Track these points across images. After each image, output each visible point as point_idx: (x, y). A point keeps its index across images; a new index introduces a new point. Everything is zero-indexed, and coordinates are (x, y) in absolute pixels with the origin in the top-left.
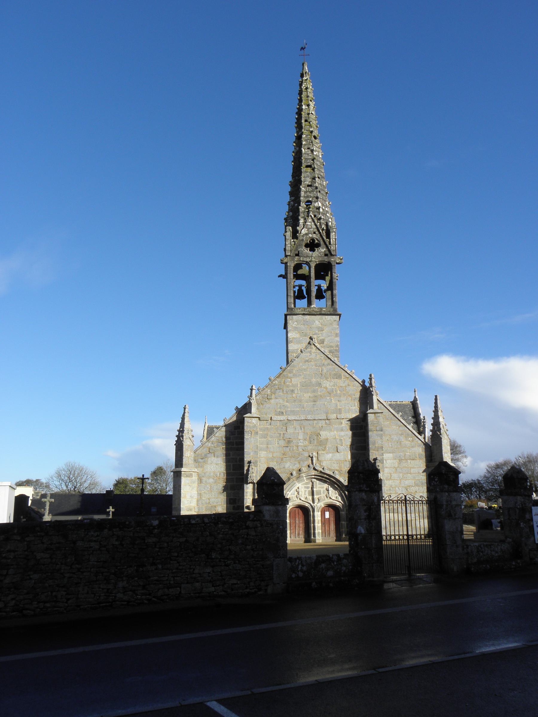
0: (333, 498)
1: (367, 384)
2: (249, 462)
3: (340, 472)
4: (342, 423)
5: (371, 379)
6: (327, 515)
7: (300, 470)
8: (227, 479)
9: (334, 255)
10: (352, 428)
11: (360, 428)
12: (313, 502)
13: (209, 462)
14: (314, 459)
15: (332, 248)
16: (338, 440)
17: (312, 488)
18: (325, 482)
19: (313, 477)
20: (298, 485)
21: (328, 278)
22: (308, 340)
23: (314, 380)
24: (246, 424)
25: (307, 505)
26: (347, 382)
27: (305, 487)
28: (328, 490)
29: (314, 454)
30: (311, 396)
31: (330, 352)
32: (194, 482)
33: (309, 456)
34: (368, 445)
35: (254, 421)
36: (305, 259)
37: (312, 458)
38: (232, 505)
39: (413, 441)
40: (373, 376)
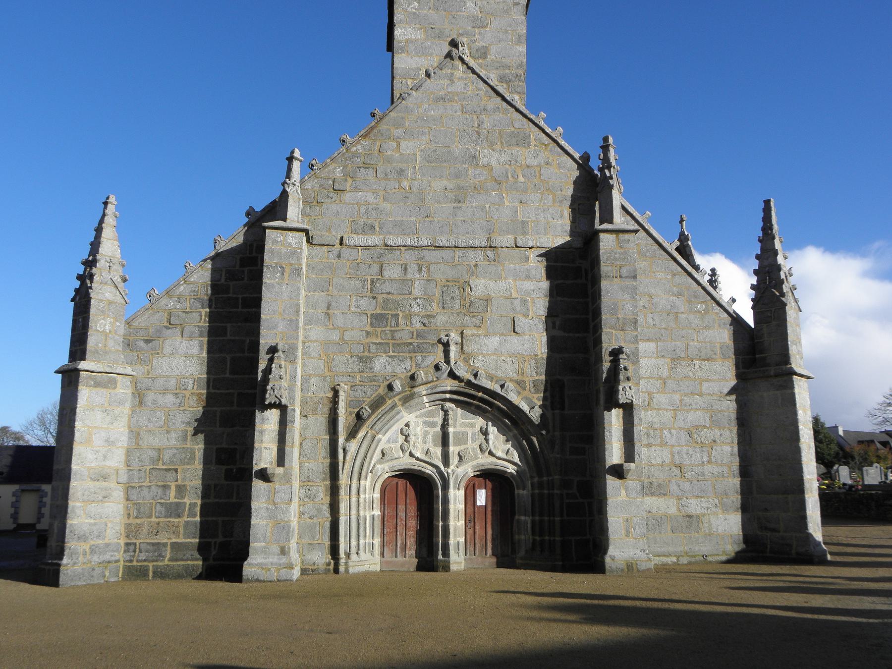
0: (500, 454)
1: (595, 164)
2: (273, 350)
3: (520, 384)
4: (527, 259)
5: (605, 148)
6: (482, 497)
7: (412, 377)
8: (209, 397)
10: (551, 273)
11: (574, 277)
12: (446, 462)
13: (167, 349)
14: (453, 349)
16: (517, 303)
17: (445, 426)
18: (477, 411)
19: (448, 396)
20: (407, 416)
22: (446, 48)
23: (458, 149)
24: (268, 245)
25: (429, 470)
26: (544, 155)
27: (426, 424)
28: (485, 433)
29: (453, 335)
30: (451, 185)
31: (502, 79)
32: (121, 403)
33: (440, 341)
34: (597, 313)
35: (293, 239)
37: (446, 345)
38: (224, 468)
39: (707, 311)
40: (611, 140)
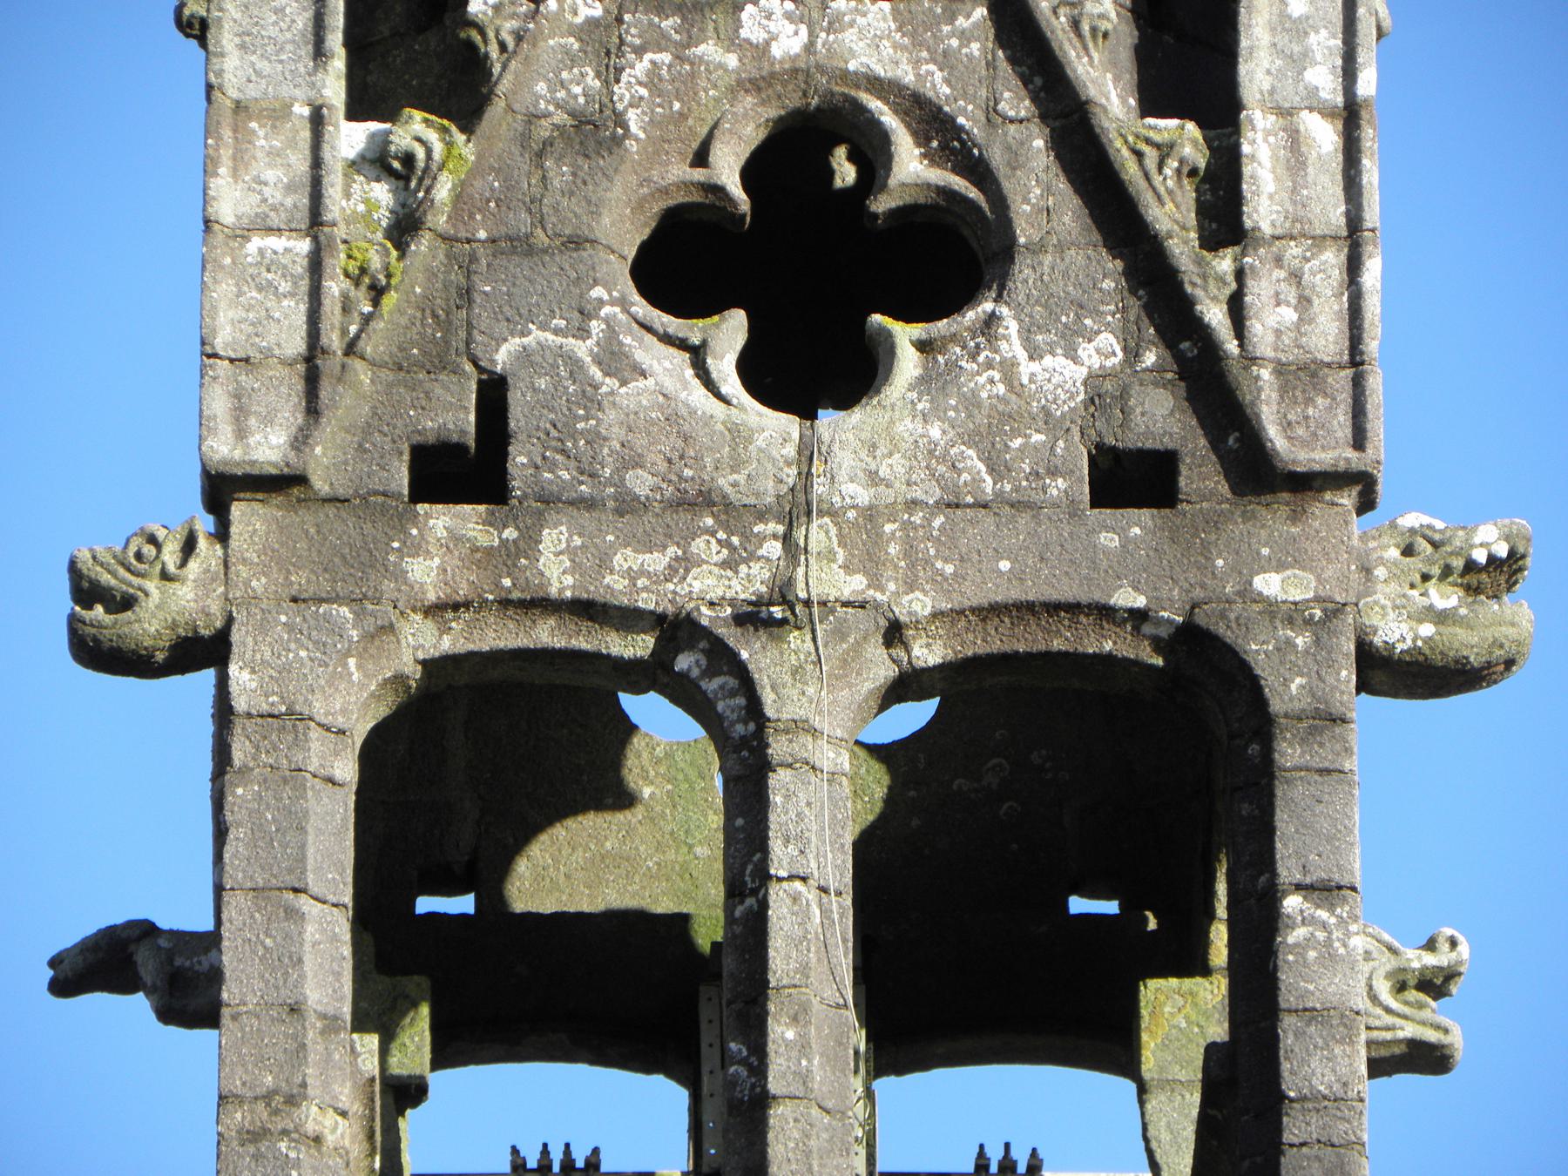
9: (1307, 484)
15: (1280, 315)
21: (1182, 1016)
36: (637, 573)
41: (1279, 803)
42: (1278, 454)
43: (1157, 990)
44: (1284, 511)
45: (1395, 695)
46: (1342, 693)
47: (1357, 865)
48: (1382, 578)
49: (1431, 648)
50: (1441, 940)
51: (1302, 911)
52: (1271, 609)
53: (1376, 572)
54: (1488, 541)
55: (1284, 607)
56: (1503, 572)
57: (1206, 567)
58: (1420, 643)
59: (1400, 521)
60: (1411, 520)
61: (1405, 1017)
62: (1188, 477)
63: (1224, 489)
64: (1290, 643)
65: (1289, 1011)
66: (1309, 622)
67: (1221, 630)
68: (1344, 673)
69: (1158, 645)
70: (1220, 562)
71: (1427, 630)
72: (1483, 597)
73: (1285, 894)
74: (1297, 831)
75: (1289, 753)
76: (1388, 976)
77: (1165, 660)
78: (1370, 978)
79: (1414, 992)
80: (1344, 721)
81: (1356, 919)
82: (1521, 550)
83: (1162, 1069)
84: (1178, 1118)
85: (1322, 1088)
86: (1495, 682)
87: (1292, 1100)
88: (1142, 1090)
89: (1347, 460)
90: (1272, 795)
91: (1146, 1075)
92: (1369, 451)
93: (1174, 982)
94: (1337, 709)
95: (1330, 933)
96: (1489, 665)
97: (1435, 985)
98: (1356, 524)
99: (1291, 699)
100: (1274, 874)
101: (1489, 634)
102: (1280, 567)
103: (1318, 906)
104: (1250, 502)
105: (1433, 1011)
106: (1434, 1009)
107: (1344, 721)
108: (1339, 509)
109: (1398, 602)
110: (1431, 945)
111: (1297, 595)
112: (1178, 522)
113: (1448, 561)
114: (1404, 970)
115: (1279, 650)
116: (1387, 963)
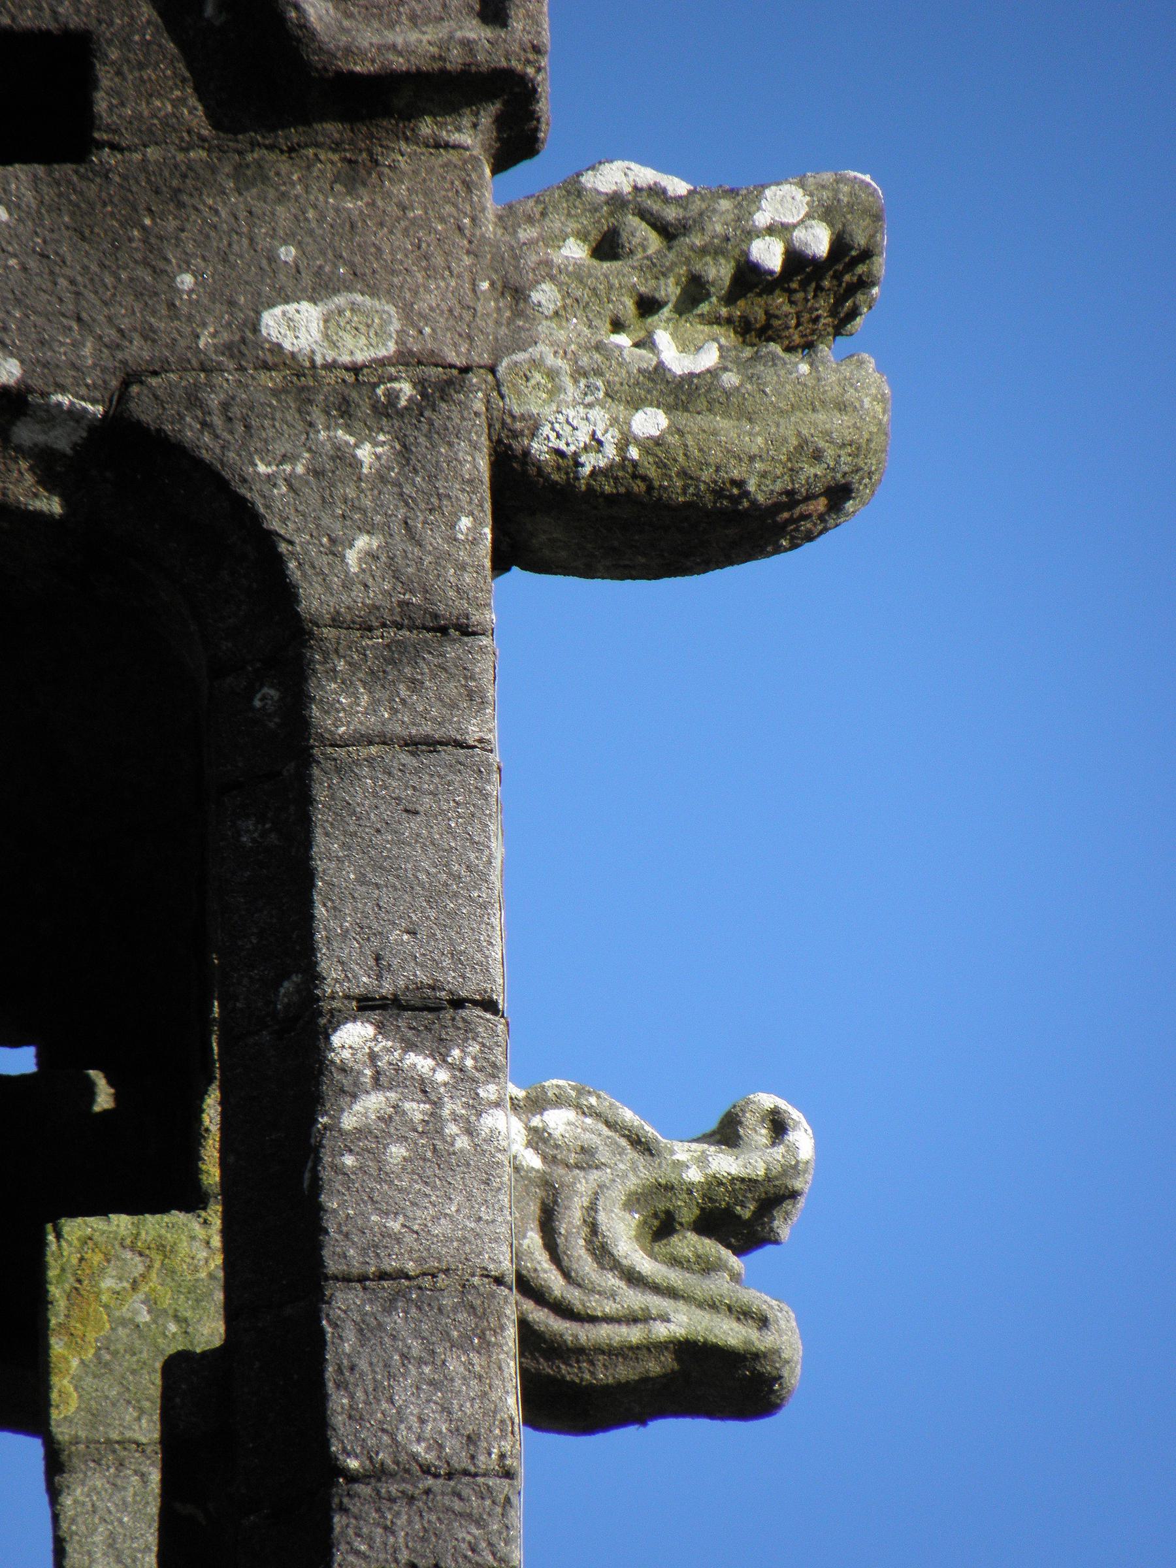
9: (385, 102)
41: (321, 816)
42: (313, 34)
43: (85, 1240)
44: (329, 162)
45: (588, 572)
46: (463, 567)
47: (497, 953)
48: (549, 308)
49: (661, 465)
50: (750, 1119)
51: (373, 1057)
52: (300, 379)
53: (535, 296)
54: (786, 219)
55: (330, 378)
56: (823, 291)
57: (155, 291)
58: (634, 453)
59: (589, 180)
60: (614, 177)
61: (671, 1293)
62: (112, 92)
63: (195, 115)
64: (344, 458)
65: (347, 1279)
66: (387, 410)
67: (190, 432)
68: (465, 523)
69: (50, 469)
70: (186, 281)
71: (650, 422)
72: (775, 348)
73: (337, 1020)
74: (362, 880)
75: (344, 705)
76: (633, 1202)
77: (66, 502)
78: (592, 1208)
79: (692, 1237)
80: (466, 631)
81: (493, 1072)
82: (861, 240)
83: (95, 1417)
84: (122, 1514)
85: (419, 1449)
86: (810, 537)
87: (352, 1478)
88: (55, 1464)
89: (467, 44)
90: (306, 800)
91: (62, 1433)
92: (517, 24)
93: (122, 1222)
94: (450, 605)
95: (437, 1104)
96: (791, 499)
97: (740, 1219)
98: (491, 192)
99: (347, 585)
100: (313, 977)
101: (788, 430)
102: (320, 288)
103: (409, 1046)
104: (254, 145)
105: (735, 1277)
106: (737, 1274)
107: (466, 631)
108: (452, 156)
109: (584, 361)
110: (727, 1133)
111: (358, 349)
112: (92, 190)
113: (698, 267)
114: (669, 1188)
115: (318, 473)
116: (627, 1173)
